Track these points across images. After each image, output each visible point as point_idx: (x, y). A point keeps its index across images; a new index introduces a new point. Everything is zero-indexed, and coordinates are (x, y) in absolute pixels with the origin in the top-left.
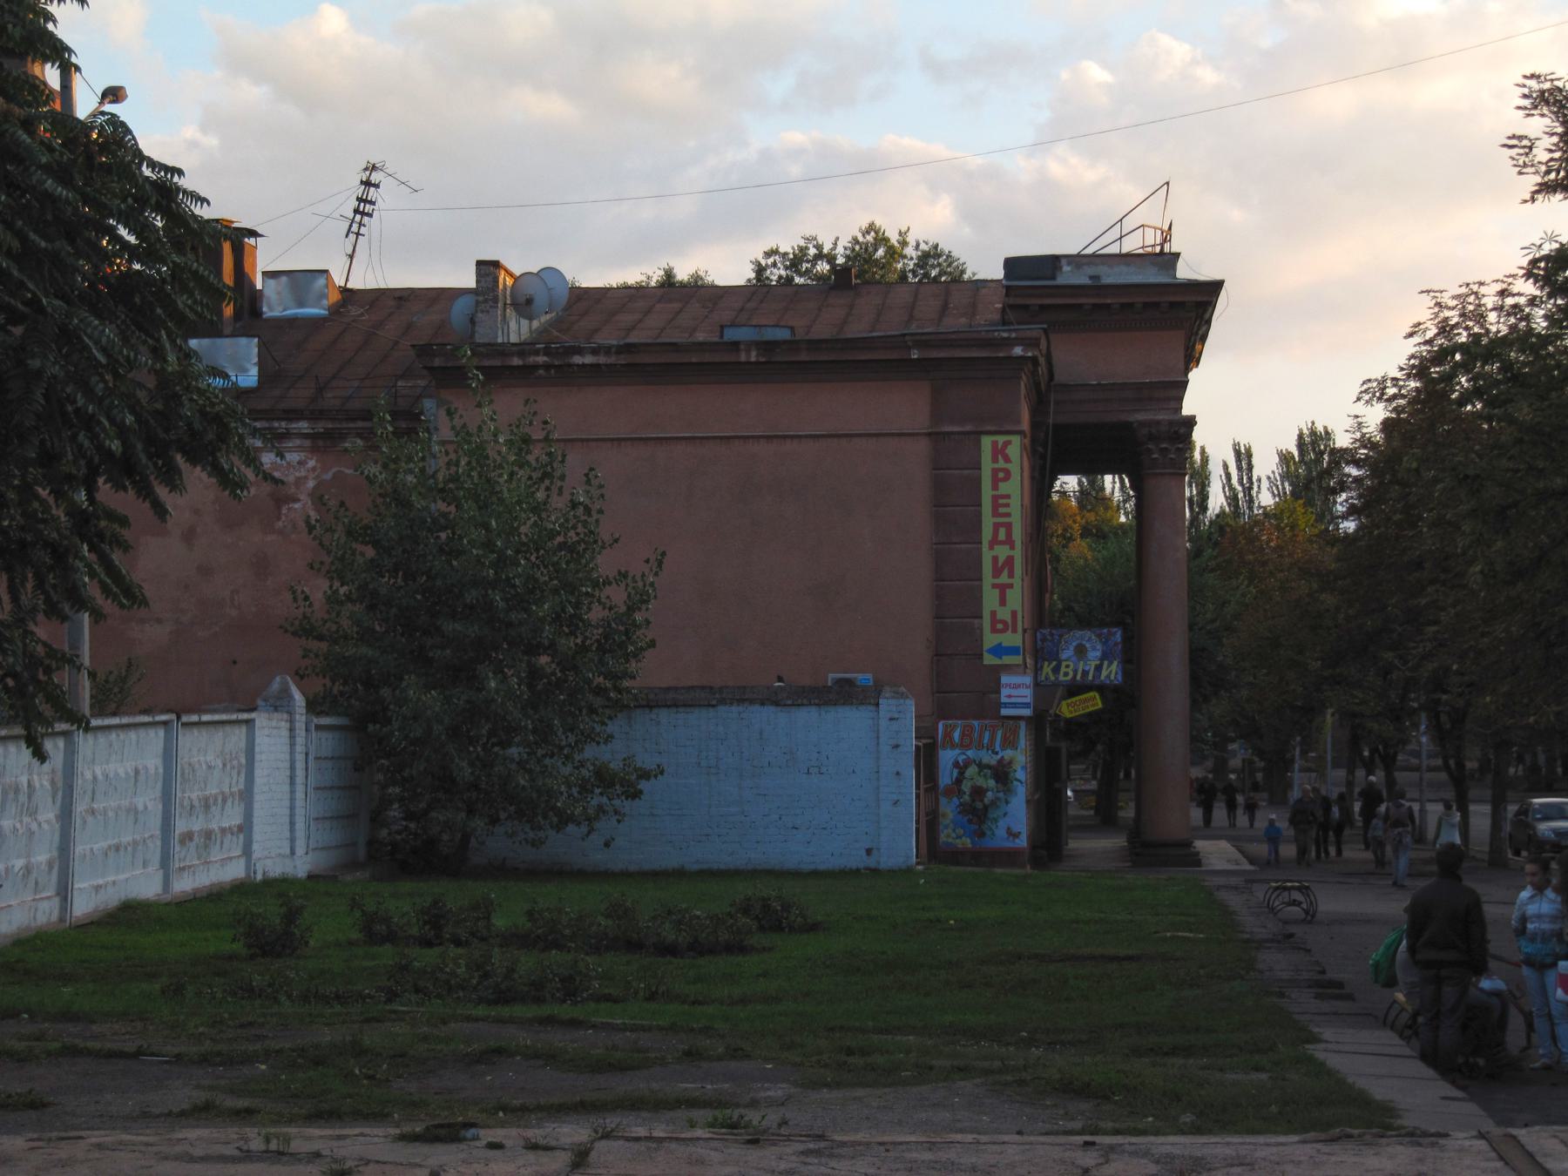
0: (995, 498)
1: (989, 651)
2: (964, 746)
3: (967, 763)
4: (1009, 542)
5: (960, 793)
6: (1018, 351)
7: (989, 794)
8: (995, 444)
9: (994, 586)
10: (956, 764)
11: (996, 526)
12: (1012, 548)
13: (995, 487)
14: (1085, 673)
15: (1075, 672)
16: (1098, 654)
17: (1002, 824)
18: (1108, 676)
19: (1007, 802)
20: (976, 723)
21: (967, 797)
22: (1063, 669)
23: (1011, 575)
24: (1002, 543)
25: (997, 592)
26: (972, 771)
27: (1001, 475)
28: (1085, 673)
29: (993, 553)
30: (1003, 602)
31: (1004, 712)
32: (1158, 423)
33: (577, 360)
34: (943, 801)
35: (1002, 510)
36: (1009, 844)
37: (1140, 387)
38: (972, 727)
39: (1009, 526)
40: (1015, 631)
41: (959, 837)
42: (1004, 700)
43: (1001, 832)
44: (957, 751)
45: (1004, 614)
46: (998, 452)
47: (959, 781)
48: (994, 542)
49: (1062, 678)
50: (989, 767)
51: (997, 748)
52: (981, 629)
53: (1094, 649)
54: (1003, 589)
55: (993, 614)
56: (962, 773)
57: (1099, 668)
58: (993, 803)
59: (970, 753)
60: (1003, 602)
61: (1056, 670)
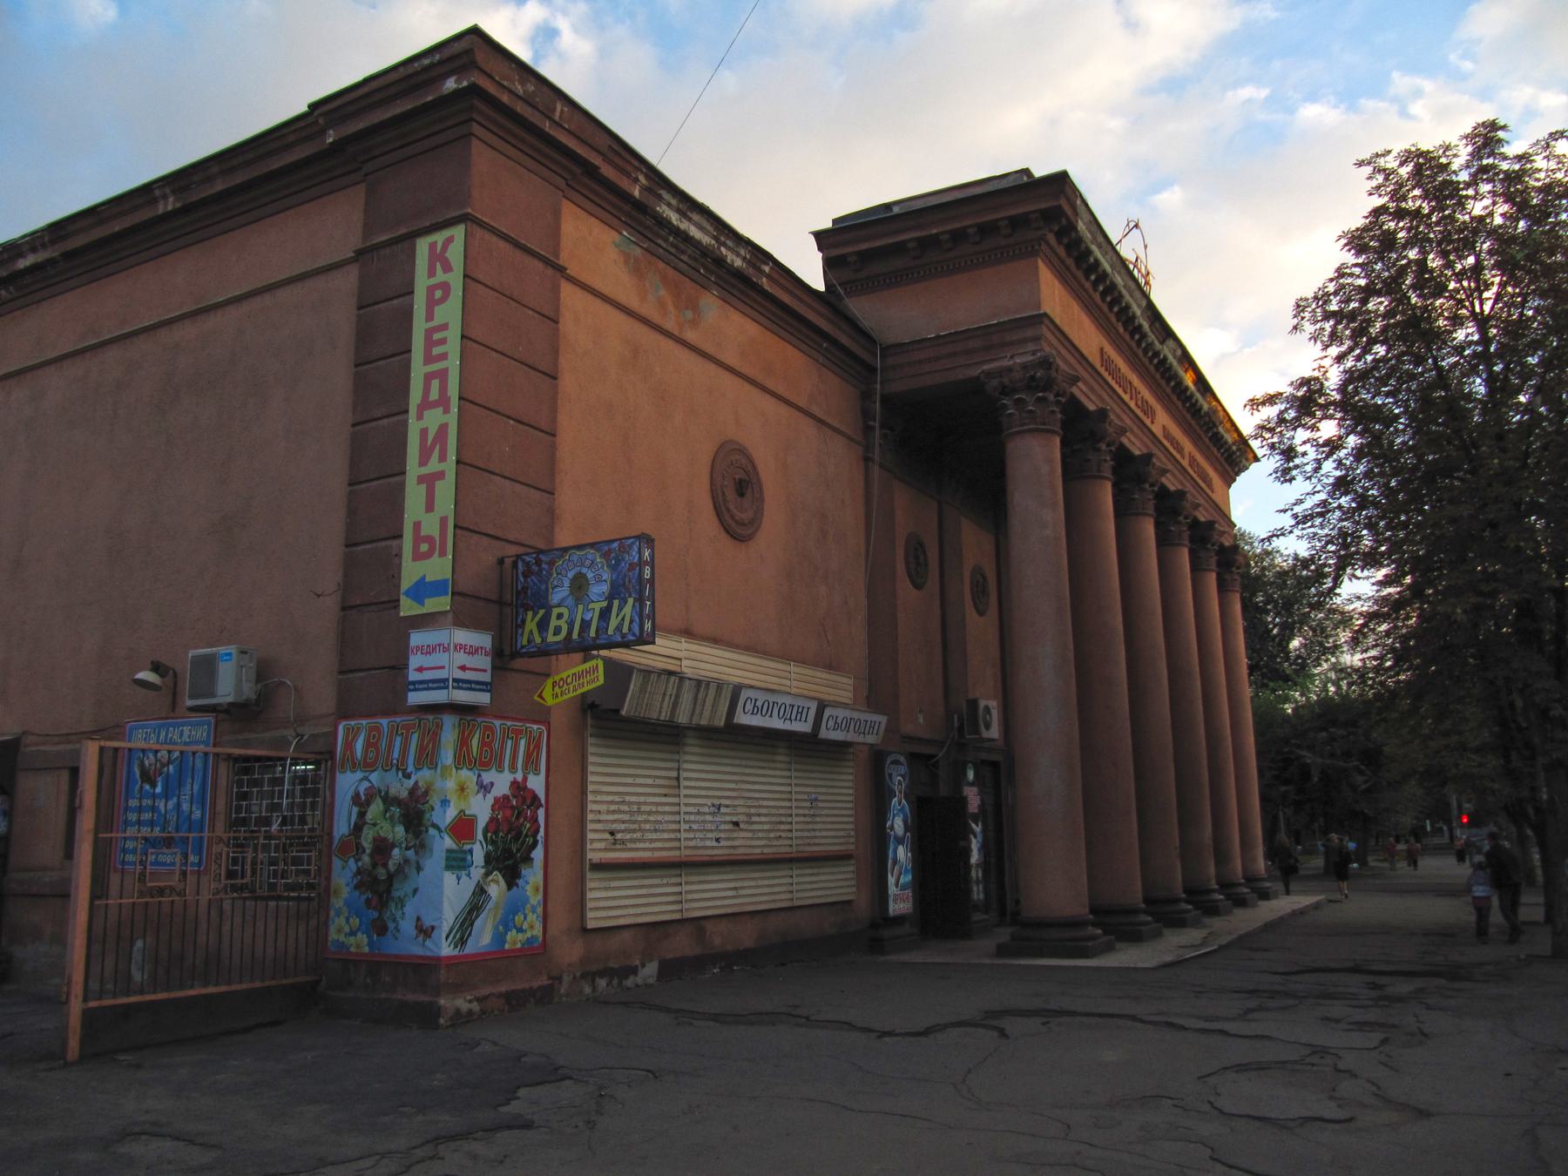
0: (429, 333)
1: (407, 594)
2: (368, 766)
3: (372, 794)
4: (443, 402)
5: (359, 849)
6: (451, 84)
7: (396, 851)
8: (433, 246)
9: (421, 479)
10: (356, 799)
11: (429, 377)
12: (447, 411)
13: (430, 316)
14: (585, 625)
15: (571, 624)
16: (605, 588)
17: (410, 909)
18: (619, 628)
19: (419, 869)
20: (384, 722)
21: (366, 859)
22: (554, 623)
23: (443, 458)
24: (434, 405)
25: (423, 487)
26: (376, 808)
27: (438, 294)
28: (585, 625)
29: (422, 424)
30: (430, 507)
31: (415, 698)
32: (1010, 370)
33: (22, 264)
34: (337, 863)
35: (436, 351)
36: (417, 950)
37: (986, 330)
38: (377, 729)
39: (443, 375)
40: (443, 554)
41: (353, 933)
42: (413, 676)
43: (407, 926)
44: (359, 775)
45: (431, 527)
46: (438, 259)
47: (358, 829)
48: (425, 405)
49: (551, 638)
50: (397, 802)
51: (410, 769)
52: (399, 555)
53: (599, 580)
54: (429, 481)
55: (417, 525)
56: (362, 815)
57: (605, 614)
58: (400, 869)
59: (374, 777)
60: (430, 507)
61: (543, 625)
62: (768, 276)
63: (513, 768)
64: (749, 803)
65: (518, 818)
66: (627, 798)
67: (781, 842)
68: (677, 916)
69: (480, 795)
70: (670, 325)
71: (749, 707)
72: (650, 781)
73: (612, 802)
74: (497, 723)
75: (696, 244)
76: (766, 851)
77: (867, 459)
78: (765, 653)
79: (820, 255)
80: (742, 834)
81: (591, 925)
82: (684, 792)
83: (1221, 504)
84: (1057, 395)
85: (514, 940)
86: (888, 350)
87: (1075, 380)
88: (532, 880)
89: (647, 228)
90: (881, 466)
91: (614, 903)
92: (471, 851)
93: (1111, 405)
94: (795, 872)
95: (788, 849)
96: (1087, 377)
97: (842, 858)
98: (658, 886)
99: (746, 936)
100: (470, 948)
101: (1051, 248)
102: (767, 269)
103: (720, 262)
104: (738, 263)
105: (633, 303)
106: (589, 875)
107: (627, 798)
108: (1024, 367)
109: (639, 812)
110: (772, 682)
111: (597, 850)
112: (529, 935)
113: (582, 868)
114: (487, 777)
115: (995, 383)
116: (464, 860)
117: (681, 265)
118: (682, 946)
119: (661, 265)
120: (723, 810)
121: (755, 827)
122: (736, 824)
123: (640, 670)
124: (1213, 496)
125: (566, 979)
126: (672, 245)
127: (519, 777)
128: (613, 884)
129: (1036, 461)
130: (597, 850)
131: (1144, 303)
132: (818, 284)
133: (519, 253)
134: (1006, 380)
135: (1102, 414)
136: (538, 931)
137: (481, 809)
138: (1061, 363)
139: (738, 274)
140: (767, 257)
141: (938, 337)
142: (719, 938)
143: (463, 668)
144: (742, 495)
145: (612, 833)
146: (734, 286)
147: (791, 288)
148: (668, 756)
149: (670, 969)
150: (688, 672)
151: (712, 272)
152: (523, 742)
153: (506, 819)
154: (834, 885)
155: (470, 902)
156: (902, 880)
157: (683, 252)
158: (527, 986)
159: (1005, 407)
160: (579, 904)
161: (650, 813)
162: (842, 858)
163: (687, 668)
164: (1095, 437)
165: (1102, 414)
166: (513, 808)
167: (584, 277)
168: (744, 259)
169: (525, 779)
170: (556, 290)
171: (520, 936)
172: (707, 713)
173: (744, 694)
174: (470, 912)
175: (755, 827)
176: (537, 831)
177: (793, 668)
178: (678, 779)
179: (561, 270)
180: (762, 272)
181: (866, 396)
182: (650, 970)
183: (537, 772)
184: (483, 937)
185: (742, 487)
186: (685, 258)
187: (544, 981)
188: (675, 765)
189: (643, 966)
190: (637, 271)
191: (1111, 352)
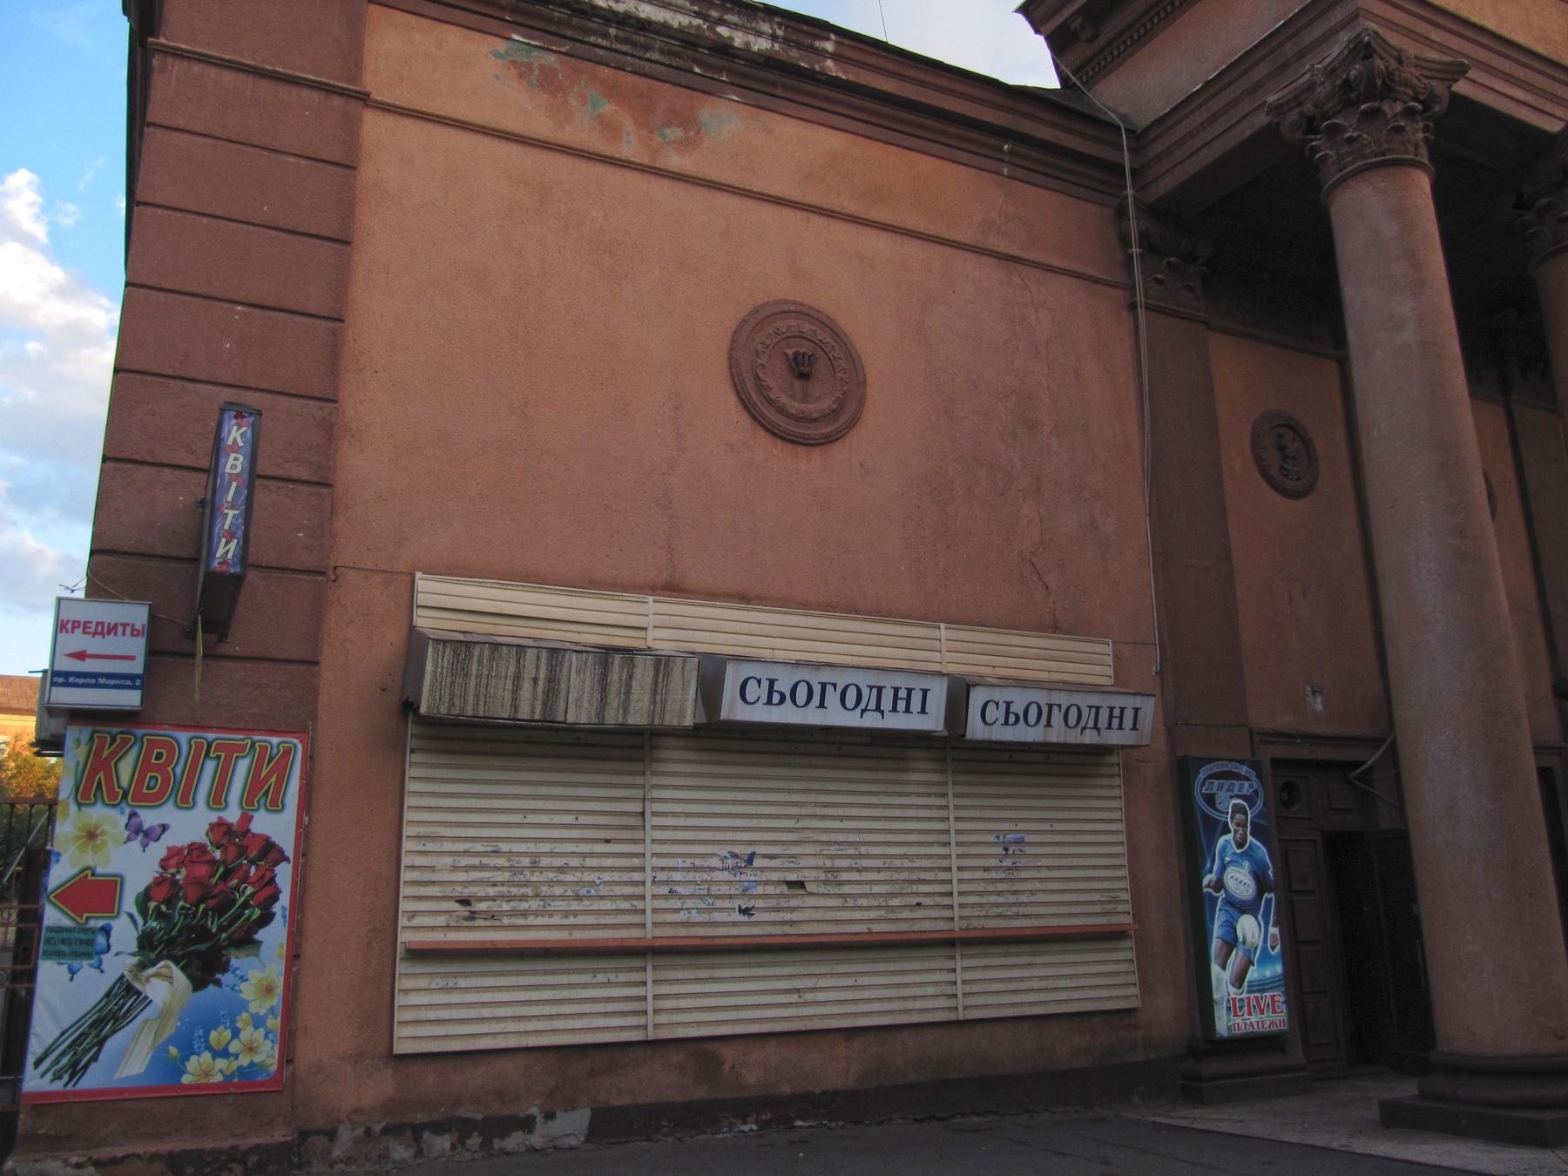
32: (1311, 87)
62: (834, 57)
63: (218, 798)
64: (833, 850)
65: (225, 877)
66: (505, 847)
67: (919, 913)
68: (637, 1036)
69: (136, 844)
70: (629, 148)
71: (992, 713)
72: (569, 819)
73: (466, 853)
74: (183, 737)
75: (664, 30)
76: (876, 928)
77: (1133, 307)
78: (877, 612)
79: (1041, 39)
80: (811, 902)
81: (400, 1048)
82: (651, 834)
85: (199, 1068)
86: (1140, 138)
88: (255, 976)
89: (559, 23)
90: (1148, 308)
91: (437, 1013)
92: (106, 931)
94: (959, 964)
95: (942, 925)
96: (1482, 55)
97: (1113, 935)
98: (585, 986)
99: (836, 1071)
100: (93, 1079)
102: (829, 46)
103: (724, 49)
104: (760, 44)
105: (542, 127)
106: (401, 968)
107: (466, 841)
108: (1331, 72)
109: (535, 867)
110: (1037, 669)
111: (423, 922)
112: (244, 1061)
113: (385, 955)
114: (149, 818)
115: (1292, 117)
116: (90, 943)
117: (648, 66)
118: (658, 1083)
119: (606, 72)
120: (757, 863)
121: (846, 889)
122: (800, 884)
123: (437, 641)
125: (345, 1135)
126: (617, 39)
127: (232, 815)
128: (463, 982)
130: (423, 922)
132: (1048, 79)
133: (264, 84)
134: (1308, 108)
136: (268, 1054)
137: (136, 868)
138: (1394, 39)
139: (767, 62)
140: (823, 28)
141: (1207, 84)
142: (752, 1074)
143: (81, 656)
144: (804, 377)
145: (465, 902)
146: (773, 84)
147: (891, 66)
148: (629, 780)
149: (610, 1125)
150: (665, 647)
151: (720, 70)
152: (243, 767)
153: (193, 881)
154: (1094, 982)
155: (99, 1007)
156: (1253, 974)
157: (647, 48)
158: (226, 1144)
159: (1315, 150)
160: (383, 1015)
161: (562, 870)
162: (1113, 935)
163: (661, 641)
166: (213, 863)
167: (403, 98)
168: (774, 37)
169: (246, 818)
170: (352, 128)
171: (221, 1063)
172: (645, 704)
173: (977, 698)
174: (98, 1024)
175: (846, 889)
176: (274, 897)
177: (943, 631)
178: (643, 814)
179: (364, 99)
180: (823, 53)
181: (1121, 213)
182: (571, 1125)
183: (276, 805)
184: (128, 1060)
185: (801, 368)
186: (656, 56)
187: (279, 1135)
188: (638, 793)
189: (549, 1116)
190: (548, 82)
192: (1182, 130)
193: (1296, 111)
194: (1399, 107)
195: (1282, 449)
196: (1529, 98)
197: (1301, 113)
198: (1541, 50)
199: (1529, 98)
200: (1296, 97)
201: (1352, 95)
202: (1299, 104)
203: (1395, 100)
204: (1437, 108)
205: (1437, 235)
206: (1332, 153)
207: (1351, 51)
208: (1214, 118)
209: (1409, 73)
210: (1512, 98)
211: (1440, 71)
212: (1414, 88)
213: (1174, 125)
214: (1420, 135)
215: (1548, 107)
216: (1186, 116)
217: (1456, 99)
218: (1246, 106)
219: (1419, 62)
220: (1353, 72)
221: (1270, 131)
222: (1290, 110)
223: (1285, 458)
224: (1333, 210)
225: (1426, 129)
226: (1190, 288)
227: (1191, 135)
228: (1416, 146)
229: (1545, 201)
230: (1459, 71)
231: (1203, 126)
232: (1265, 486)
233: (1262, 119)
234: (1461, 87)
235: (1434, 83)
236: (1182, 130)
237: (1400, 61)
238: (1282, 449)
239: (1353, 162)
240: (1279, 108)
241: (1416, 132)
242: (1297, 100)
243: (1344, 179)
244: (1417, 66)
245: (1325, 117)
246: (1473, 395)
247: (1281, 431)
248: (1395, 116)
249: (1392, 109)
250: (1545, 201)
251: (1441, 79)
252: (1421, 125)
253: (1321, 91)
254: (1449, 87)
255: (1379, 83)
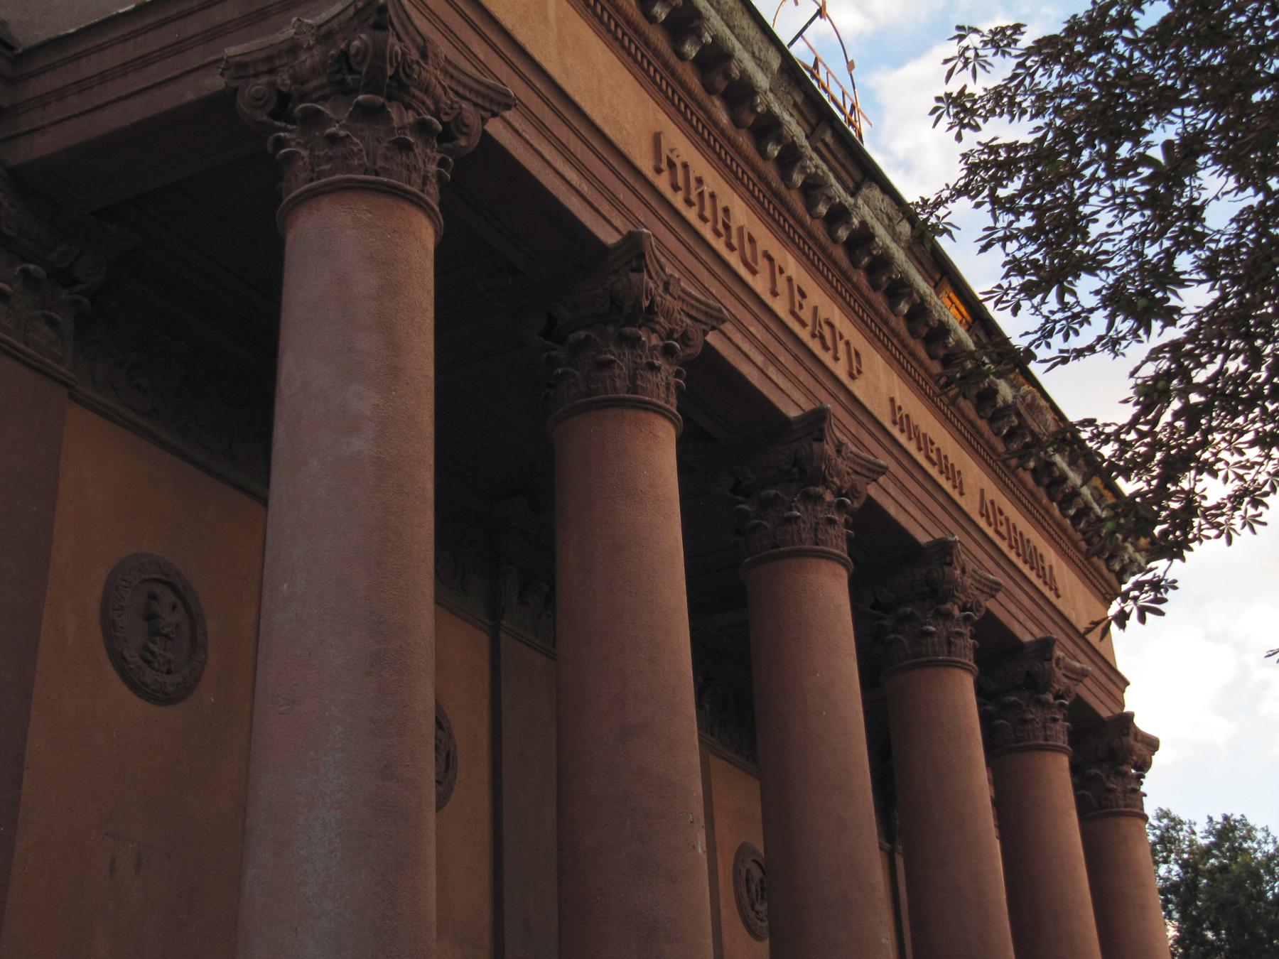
32: (293, 48)
83: (1109, 659)
84: (1057, 697)
87: (715, 319)
93: (653, 229)
101: (921, 364)
108: (326, 35)
124: (1059, 603)
129: (362, 301)
131: (776, 63)
134: (284, 80)
135: (944, 549)
159: (280, 143)
164: (1035, 684)
165: (633, 246)
191: (681, 146)
192: (89, 67)
193: (264, 79)
194: (410, 117)
195: (151, 617)
196: (584, 187)
197: (272, 85)
198: (607, 131)
199: (584, 187)
200: (270, 58)
201: (349, 78)
202: (272, 71)
203: (408, 107)
204: (463, 142)
205: (431, 314)
206: (305, 153)
207: (358, 12)
208: (142, 62)
209: (432, 75)
210: (563, 177)
211: (478, 93)
212: (437, 102)
213: (77, 57)
214: (433, 168)
215: (605, 208)
216: (100, 48)
217: (488, 141)
218: (195, 57)
219: (449, 68)
220: (356, 43)
221: (222, 102)
222: (257, 75)
223: (155, 633)
224: (290, 238)
225: (442, 163)
226: (52, 323)
227: (103, 78)
228: (425, 179)
229: (582, 334)
230: (498, 102)
231: (123, 70)
232: (109, 669)
233: (215, 82)
234: (495, 128)
235: (464, 105)
236: (89, 67)
237: (424, 56)
238: (151, 617)
239: (332, 172)
240: (240, 68)
241: (428, 159)
242: (270, 61)
243: (314, 194)
244: (445, 72)
245: (304, 97)
246: (439, 601)
247: (158, 589)
248: (403, 127)
249: (400, 117)
250: (582, 334)
251: (476, 105)
252: (438, 156)
253: (307, 60)
254: (484, 120)
255: (390, 72)
